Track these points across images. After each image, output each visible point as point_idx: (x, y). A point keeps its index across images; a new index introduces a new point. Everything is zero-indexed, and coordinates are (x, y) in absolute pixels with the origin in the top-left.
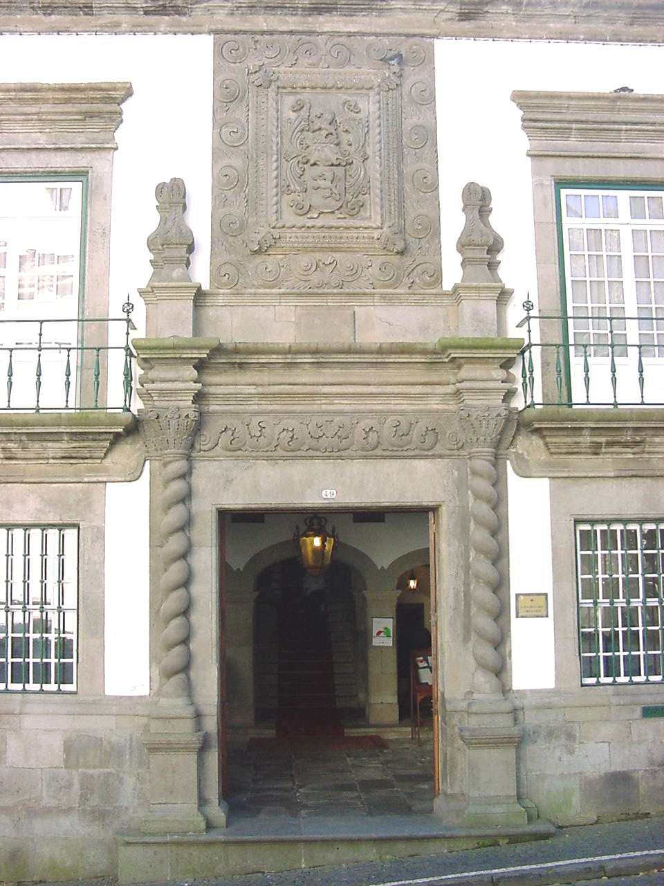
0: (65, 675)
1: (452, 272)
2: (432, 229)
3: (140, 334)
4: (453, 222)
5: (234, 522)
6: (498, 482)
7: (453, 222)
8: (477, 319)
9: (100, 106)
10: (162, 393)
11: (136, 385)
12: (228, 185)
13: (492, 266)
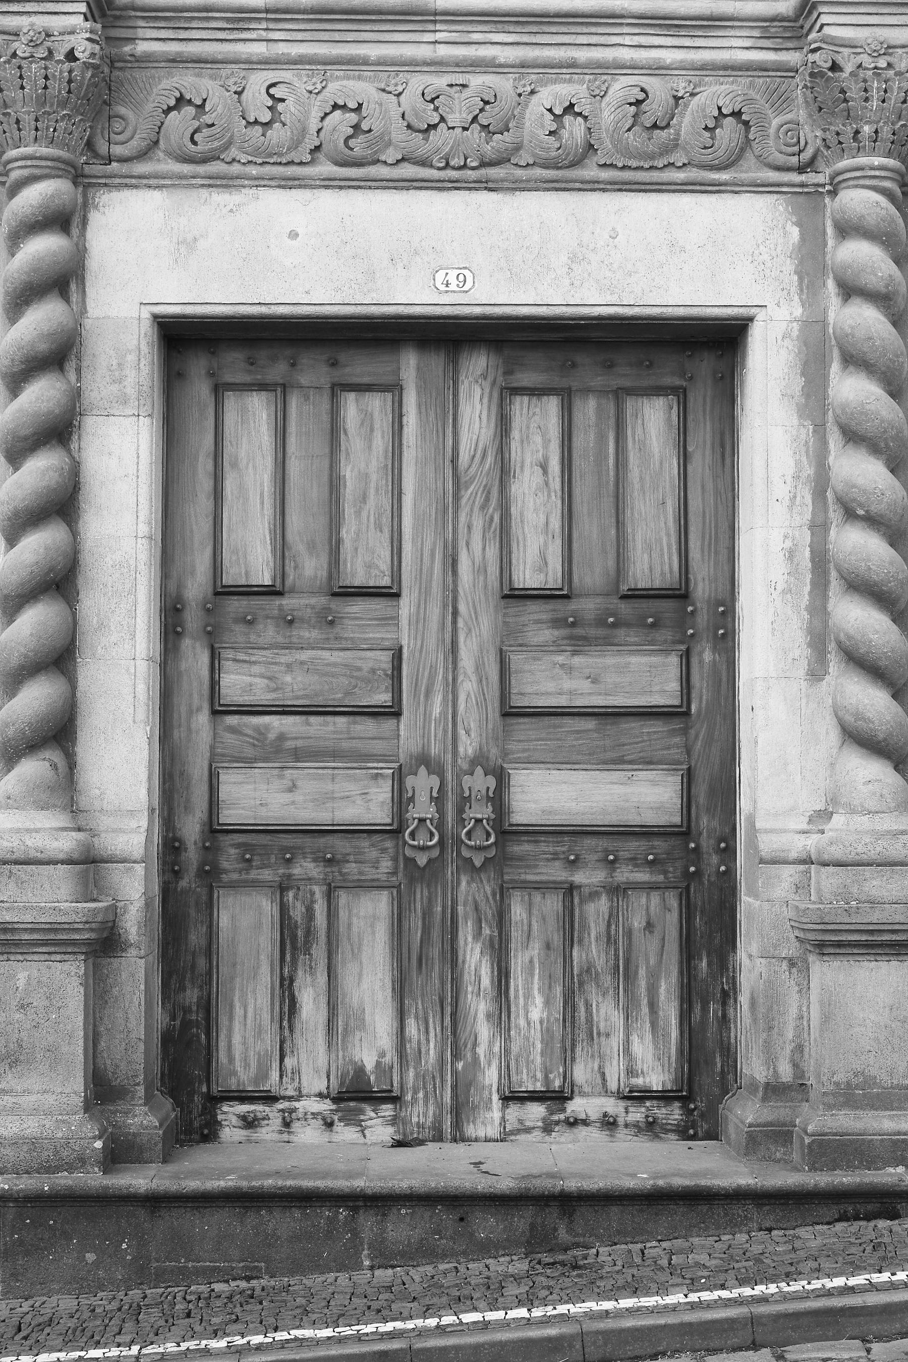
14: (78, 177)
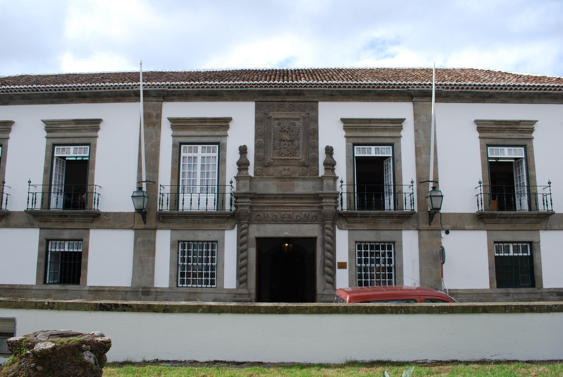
0: (213, 283)
1: (322, 172)
2: (316, 159)
3: (234, 190)
4: (322, 157)
5: (260, 241)
6: (334, 232)
7: (322, 157)
8: (328, 186)
9: (223, 123)
10: (241, 206)
11: (233, 203)
12: (258, 147)
13: (333, 170)
14: (248, 224)
